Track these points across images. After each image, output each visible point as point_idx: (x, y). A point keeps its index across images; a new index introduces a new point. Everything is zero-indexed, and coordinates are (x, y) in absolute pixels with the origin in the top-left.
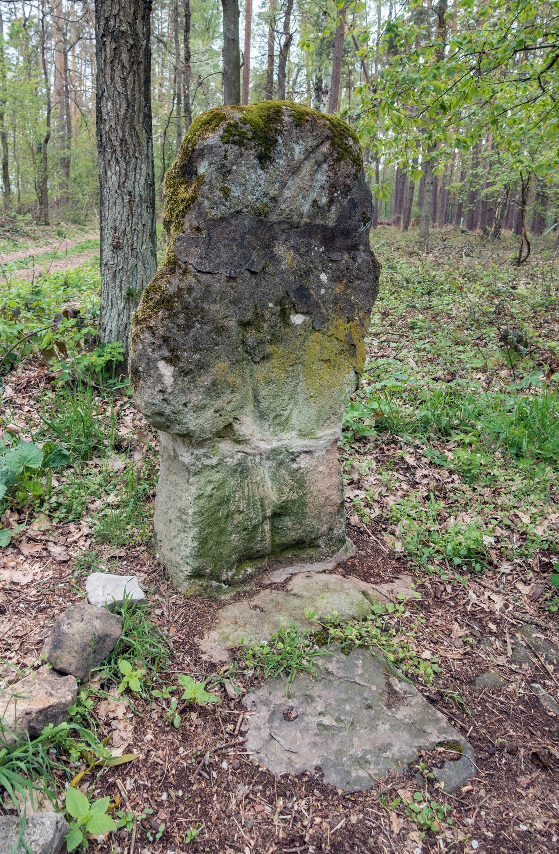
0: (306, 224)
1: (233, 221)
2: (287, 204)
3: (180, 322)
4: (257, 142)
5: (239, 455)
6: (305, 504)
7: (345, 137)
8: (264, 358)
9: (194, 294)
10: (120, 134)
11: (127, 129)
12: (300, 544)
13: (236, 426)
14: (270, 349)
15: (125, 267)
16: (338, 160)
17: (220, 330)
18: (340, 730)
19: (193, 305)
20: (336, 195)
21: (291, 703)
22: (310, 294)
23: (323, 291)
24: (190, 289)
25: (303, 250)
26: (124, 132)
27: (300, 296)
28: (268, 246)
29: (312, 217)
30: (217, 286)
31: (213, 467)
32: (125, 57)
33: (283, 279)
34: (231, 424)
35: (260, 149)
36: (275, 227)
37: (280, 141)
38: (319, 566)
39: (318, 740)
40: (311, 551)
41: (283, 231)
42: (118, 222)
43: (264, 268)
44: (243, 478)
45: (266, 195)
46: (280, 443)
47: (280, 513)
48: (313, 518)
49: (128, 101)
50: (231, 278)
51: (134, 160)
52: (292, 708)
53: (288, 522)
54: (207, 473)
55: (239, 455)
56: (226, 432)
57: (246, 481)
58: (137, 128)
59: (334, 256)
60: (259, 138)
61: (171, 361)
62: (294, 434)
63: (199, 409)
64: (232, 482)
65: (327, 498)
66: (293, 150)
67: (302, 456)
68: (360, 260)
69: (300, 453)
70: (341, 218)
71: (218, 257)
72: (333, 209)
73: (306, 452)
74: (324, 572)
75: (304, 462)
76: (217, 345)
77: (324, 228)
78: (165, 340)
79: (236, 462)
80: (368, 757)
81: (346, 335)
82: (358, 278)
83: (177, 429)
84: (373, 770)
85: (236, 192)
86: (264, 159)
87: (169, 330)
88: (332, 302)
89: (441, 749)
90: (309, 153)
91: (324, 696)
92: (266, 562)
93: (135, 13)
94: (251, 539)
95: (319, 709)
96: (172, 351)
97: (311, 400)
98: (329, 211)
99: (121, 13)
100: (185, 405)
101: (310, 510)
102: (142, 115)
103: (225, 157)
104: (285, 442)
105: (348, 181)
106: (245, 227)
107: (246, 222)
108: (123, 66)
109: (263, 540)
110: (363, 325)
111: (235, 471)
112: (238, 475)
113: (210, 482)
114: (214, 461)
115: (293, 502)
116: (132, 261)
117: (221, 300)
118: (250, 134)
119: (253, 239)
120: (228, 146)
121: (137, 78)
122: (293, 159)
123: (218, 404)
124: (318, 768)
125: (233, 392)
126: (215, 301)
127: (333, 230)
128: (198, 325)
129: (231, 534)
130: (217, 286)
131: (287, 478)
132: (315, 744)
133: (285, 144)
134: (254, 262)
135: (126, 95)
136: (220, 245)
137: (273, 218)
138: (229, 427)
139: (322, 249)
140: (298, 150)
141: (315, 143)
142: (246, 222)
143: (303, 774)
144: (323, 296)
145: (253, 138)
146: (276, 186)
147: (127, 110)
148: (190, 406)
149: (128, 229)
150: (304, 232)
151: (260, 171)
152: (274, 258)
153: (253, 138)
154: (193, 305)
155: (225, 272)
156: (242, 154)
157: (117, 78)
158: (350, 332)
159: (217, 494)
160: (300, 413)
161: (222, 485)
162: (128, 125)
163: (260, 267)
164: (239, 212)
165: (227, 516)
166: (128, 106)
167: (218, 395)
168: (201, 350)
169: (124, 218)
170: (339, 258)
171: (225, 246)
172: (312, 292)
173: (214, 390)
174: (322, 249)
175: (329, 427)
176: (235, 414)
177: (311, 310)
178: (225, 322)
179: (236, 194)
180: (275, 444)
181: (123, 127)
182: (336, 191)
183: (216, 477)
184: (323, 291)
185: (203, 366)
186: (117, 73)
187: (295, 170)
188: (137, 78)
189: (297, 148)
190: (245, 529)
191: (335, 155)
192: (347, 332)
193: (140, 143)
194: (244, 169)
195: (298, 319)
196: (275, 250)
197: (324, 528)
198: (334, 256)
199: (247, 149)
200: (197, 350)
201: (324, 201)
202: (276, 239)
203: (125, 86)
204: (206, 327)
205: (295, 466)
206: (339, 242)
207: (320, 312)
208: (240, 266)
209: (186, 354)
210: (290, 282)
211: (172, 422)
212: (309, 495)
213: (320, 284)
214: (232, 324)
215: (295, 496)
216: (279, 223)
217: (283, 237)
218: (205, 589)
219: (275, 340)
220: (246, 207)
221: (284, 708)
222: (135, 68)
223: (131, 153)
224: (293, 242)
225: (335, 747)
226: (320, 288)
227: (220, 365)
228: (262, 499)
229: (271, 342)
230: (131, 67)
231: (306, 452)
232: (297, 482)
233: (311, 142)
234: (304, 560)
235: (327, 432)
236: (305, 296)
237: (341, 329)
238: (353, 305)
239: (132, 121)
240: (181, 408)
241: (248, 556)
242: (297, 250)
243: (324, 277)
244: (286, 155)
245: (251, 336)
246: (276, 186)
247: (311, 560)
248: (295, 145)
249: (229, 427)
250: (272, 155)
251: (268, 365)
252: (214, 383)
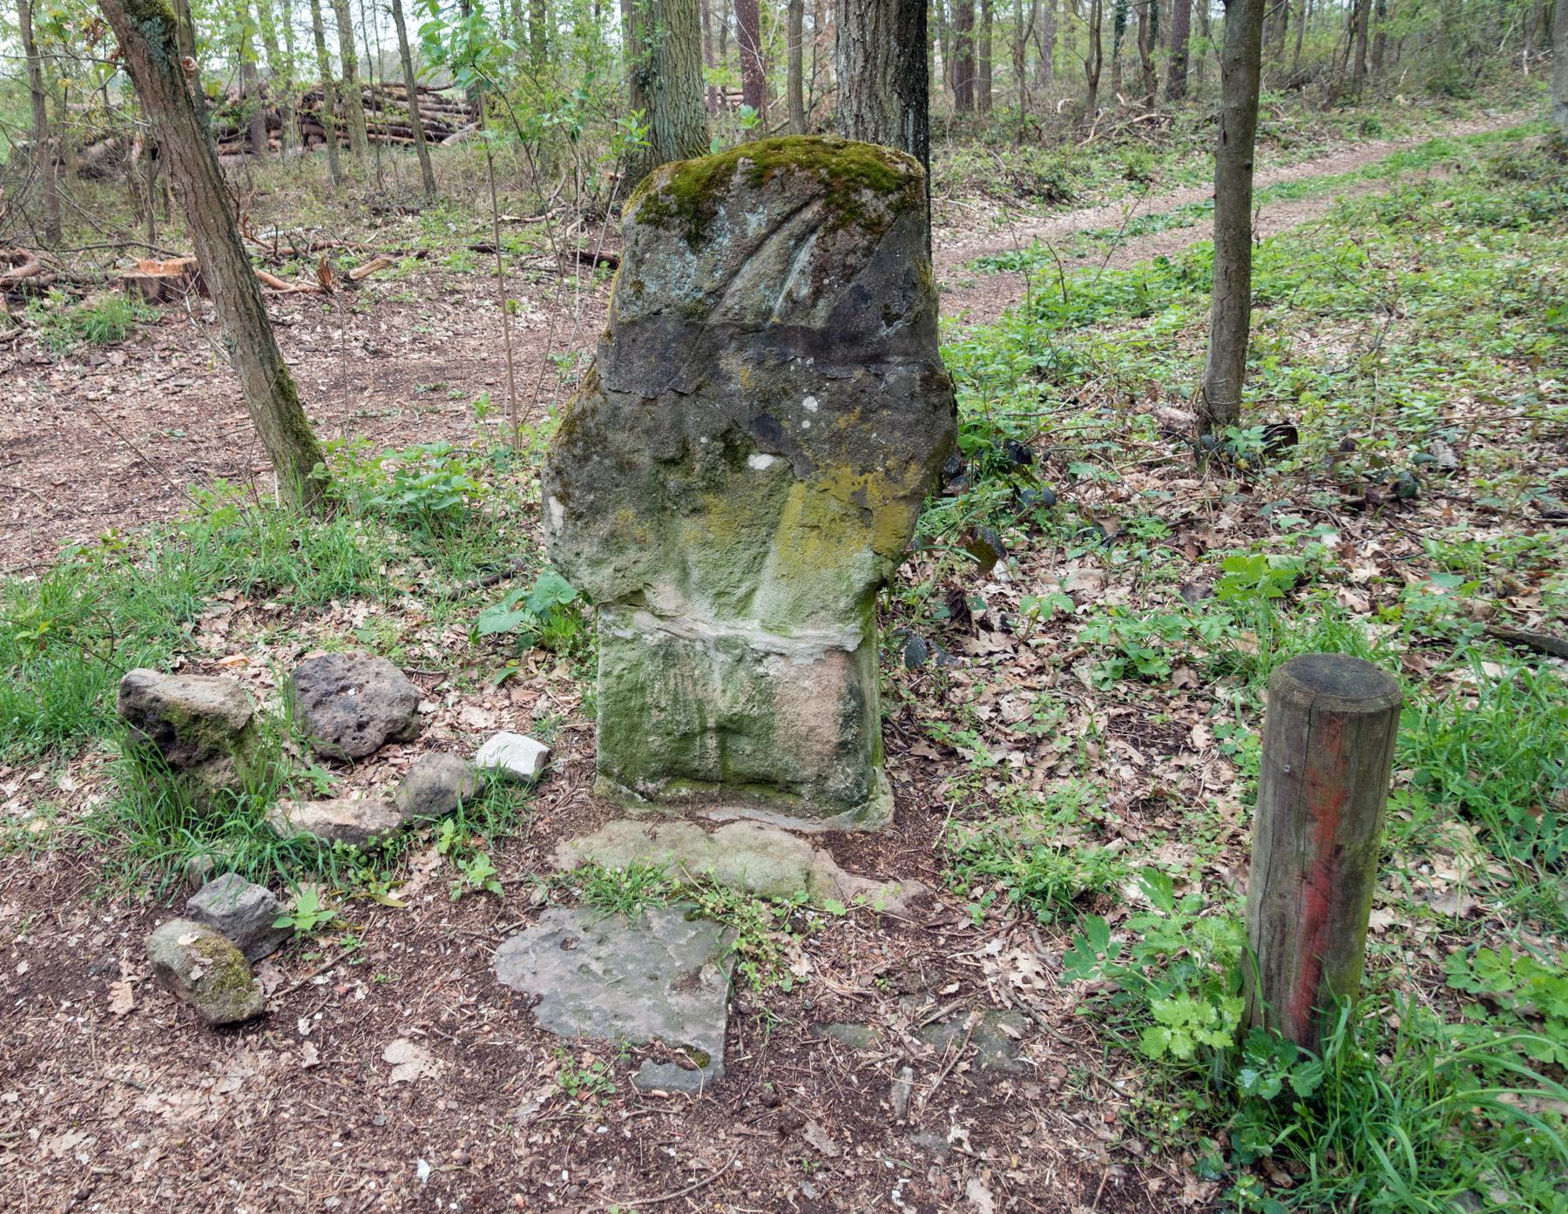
0: (775, 326)
1: (649, 325)
2: (736, 299)
3: (577, 451)
4: (685, 217)
5: (661, 634)
6: (771, 728)
7: (856, 190)
8: (694, 511)
9: (597, 418)
11: (864, 98)
12: (764, 781)
13: (648, 595)
14: (709, 499)
16: (833, 229)
17: (625, 467)
18: (599, 980)
19: (594, 431)
20: (826, 281)
21: (582, 935)
22: (781, 429)
23: (806, 424)
24: (594, 411)
25: (771, 363)
26: (860, 103)
27: (767, 426)
28: (711, 355)
29: (786, 315)
30: (627, 409)
31: (628, 642)
33: (729, 405)
35: (687, 227)
36: (718, 331)
37: (722, 212)
38: (793, 823)
39: (568, 977)
40: (790, 800)
43: (699, 388)
44: (667, 667)
46: (732, 632)
47: (729, 729)
48: (788, 750)
49: (865, 51)
50: (647, 401)
52: (577, 939)
53: (745, 745)
54: (616, 648)
55: (661, 634)
56: (634, 599)
57: (673, 671)
58: (881, 94)
60: (687, 211)
61: (563, 498)
62: (756, 623)
63: (595, 563)
64: (649, 667)
65: (812, 729)
66: (745, 222)
67: (772, 658)
68: (891, 379)
70: (834, 315)
71: (630, 372)
72: (821, 303)
73: (782, 655)
74: (794, 832)
75: (773, 667)
76: (617, 486)
77: (806, 331)
78: (559, 472)
79: (656, 642)
80: (596, 1015)
81: (854, 494)
82: (884, 406)
84: (587, 1025)
85: (651, 287)
86: (695, 240)
87: (563, 460)
88: (829, 440)
89: (681, 1051)
91: (622, 941)
92: (715, 790)
94: (685, 750)
95: (601, 954)
96: (565, 486)
97: (784, 581)
98: (814, 306)
101: (779, 735)
102: (891, 71)
103: (637, 242)
104: (741, 632)
105: (851, 260)
106: (668, 333)
107: (669, 327)
109: (702, 757)
111: (655, 654)
112: (659, 660)
113: (621, 659)
114: (628, 634)
115: (755, 720)
117: (631, 429)
118: (674, 208)
119: (682, 349)
120: (640, 227)
121: (882, 11)
122: (744, 236)
123: (619, 561)
124: (540, 998)
125: (641, 549)
126: (623, 429)
127: (824, 333)
128: (596, 458)
129: (648, 734)
130: (627, 409)
131: (746, 683)
132: (561, 978)
133: (730, 216)
134: (681, 380)
135: (863, 43)
136: (634, 357)
137: (714, 319)
138: (638, 593)
139: (810, 361)
140: (755, 223)
141: (787, 209)
142: (669, 327)
143: (521, 994)
144: (804, 432)
145: (679, 213)
147: (865, 67)
150: (768, 337)
151: (690, 257)
152: (717, 375)
153: (679, 213)
154: (594, 431)
155: (640, 393)
156: (658, 238)
158: (864, 489)
159: (628, 677)
160: (768, 596)
161: (636, 666)
162: (865, 91)
163: (692, 387)
164: (658, 313)
165: (642, 709)
166: (866, 61)
167: (622, 550)
168: (596, 489)
170: (845, 375)
171: (640, 357)
172: (785, 424)
173: (613, 543)
174: (810, 361)
175: (815, 626)
176: (647, 578)
177: (783, 451)
178: (636, 458)
179: (652, 290)
180: (723, 632)
181: (858, 94)
182: (828, 276)
183: (631, 655)
184: (806, 424)
185: (596, 511)
188: (882, 11)
190: (669, 734)
191: (831, 220)
192: (856, 488)
193: (886, 120)
194: (661, 256)
195: (760, 462)
197: (809, 772)
198: (833, 371)
199: (667, 229)
200: (590, 488)
201: (805, 291)
203: (862, 27)
204: (607, 461)
205: (760, 670)
206: (839, 352)
207: (801, 455)
208: (661, 385)
209: (577, 493)
210: (741, 409)
212: (778, 717)
213: (802, 414)
214: (644, 459)
215: (755, 712)
216: (723, 326)
217: (734, 344)
218: (613, 793)
219: (715, 487)
220: (667, 306)
221: (570, 936)
223: (870, 135)
224: (750, 352)
225: (574, 990)
226: (800, 419)
227: (622, 512)
228: (700, 702)
229: (707, 489)
232: (760, 692)
233: (779, 208)
234: (778, 809)
235: (810, 632)
236: (773, 430)
237: (844, 483)
238: (873, 450)
239: (873, 83)
240: (572, 557)
241: (674, 772)
242: (760, 363)
244: (732, 232)
245: (674, 480)
247: (788, 811)
248: (748, 216)
249: (638, 593)
250: (707, 233)
251: (702, 521)
252: (612, 534)
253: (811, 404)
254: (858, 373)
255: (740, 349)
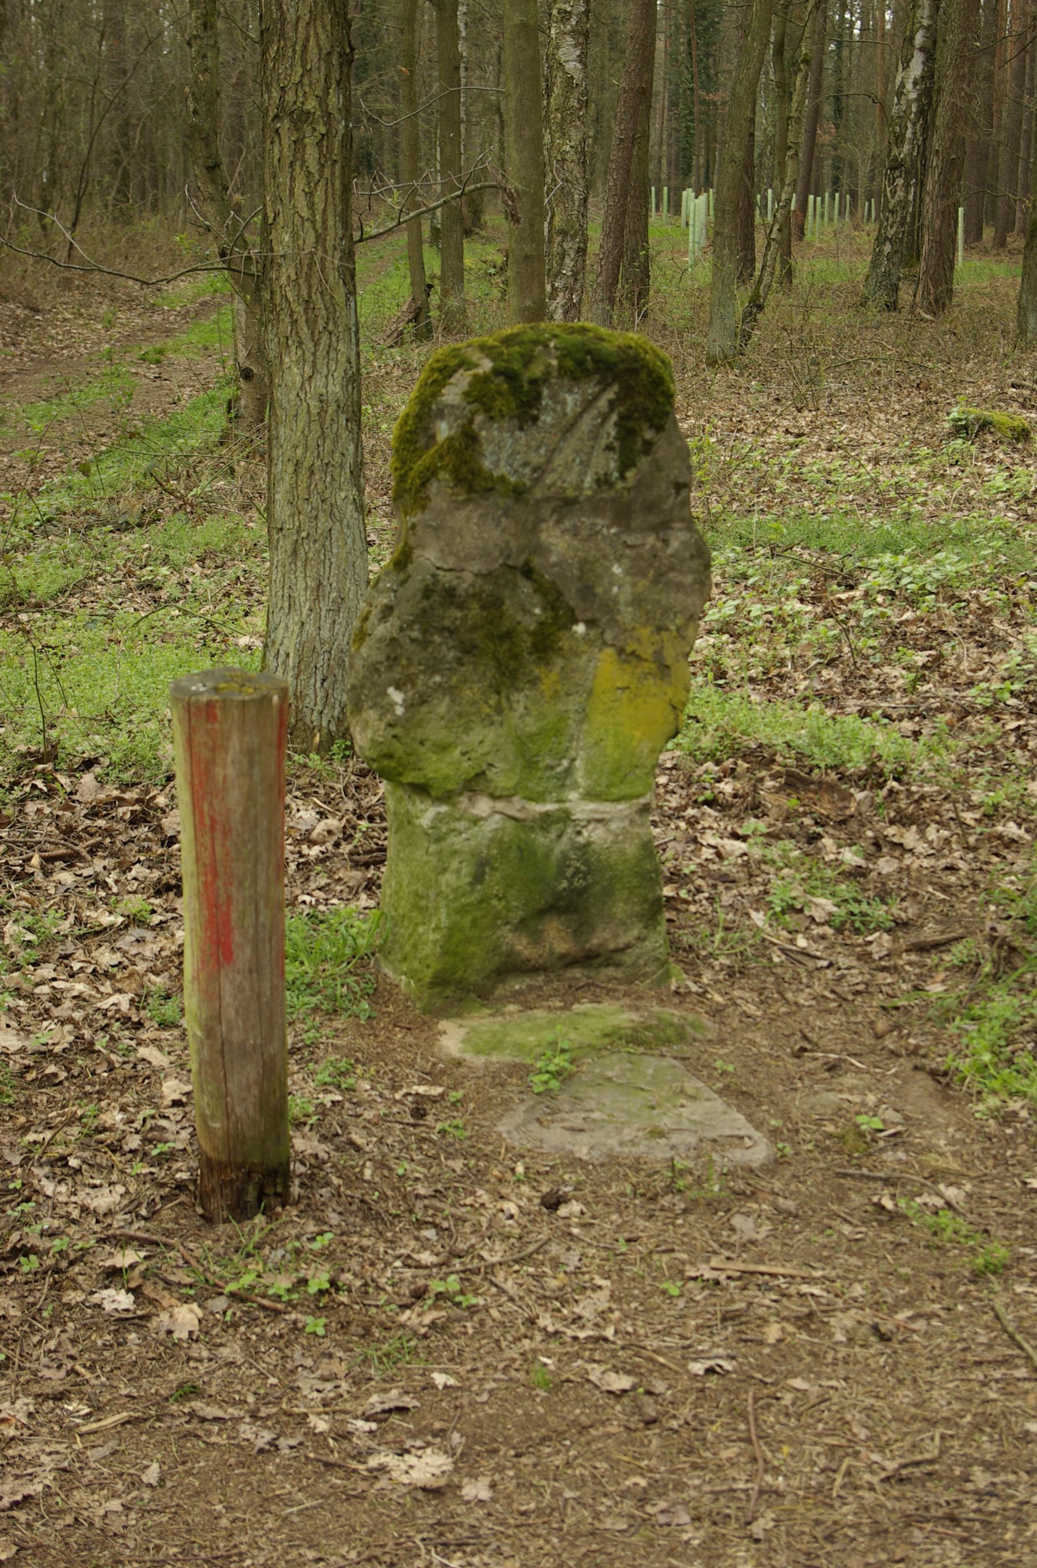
10: (304, 292)
15: (312, 532)
32: (311, 154)
34: (483, 773)
41: (554, 511)
42: (299, 451)
45: (526, 464)
51: (325, 337)
59: (631, 540)
66: (564, 403)
69: (589, 822)
73: (599, 821)
83: (410, 777)
90: (588, 405)
93: (327, 77)
99: (306, 81)
100: (422, 743)
108: (309, 173)
110: (684, 638)
116: (324, 523)
140: (571, 401)
146: (542, 451)
148: (428, 744)
149: (318, 463)
157: (298, 191)
169: (312, 444)
174: (613, 530)
186: (300, 185)
187: (570, 428)
189: (570, 399)
196: (543, 536)
202: (544, 521)
203: (311, 206)
211: (405, 767)
213: (613, 579)
222: (327, 173)
224: (567, 524)
226: (611, 584)
230: (321, 175)
231: (599, 821)
243: (616, 569)
246: (542, 451)
249: (481, 775)
253: (616, 569)
254: (651, 540)
255: (558, 522)
